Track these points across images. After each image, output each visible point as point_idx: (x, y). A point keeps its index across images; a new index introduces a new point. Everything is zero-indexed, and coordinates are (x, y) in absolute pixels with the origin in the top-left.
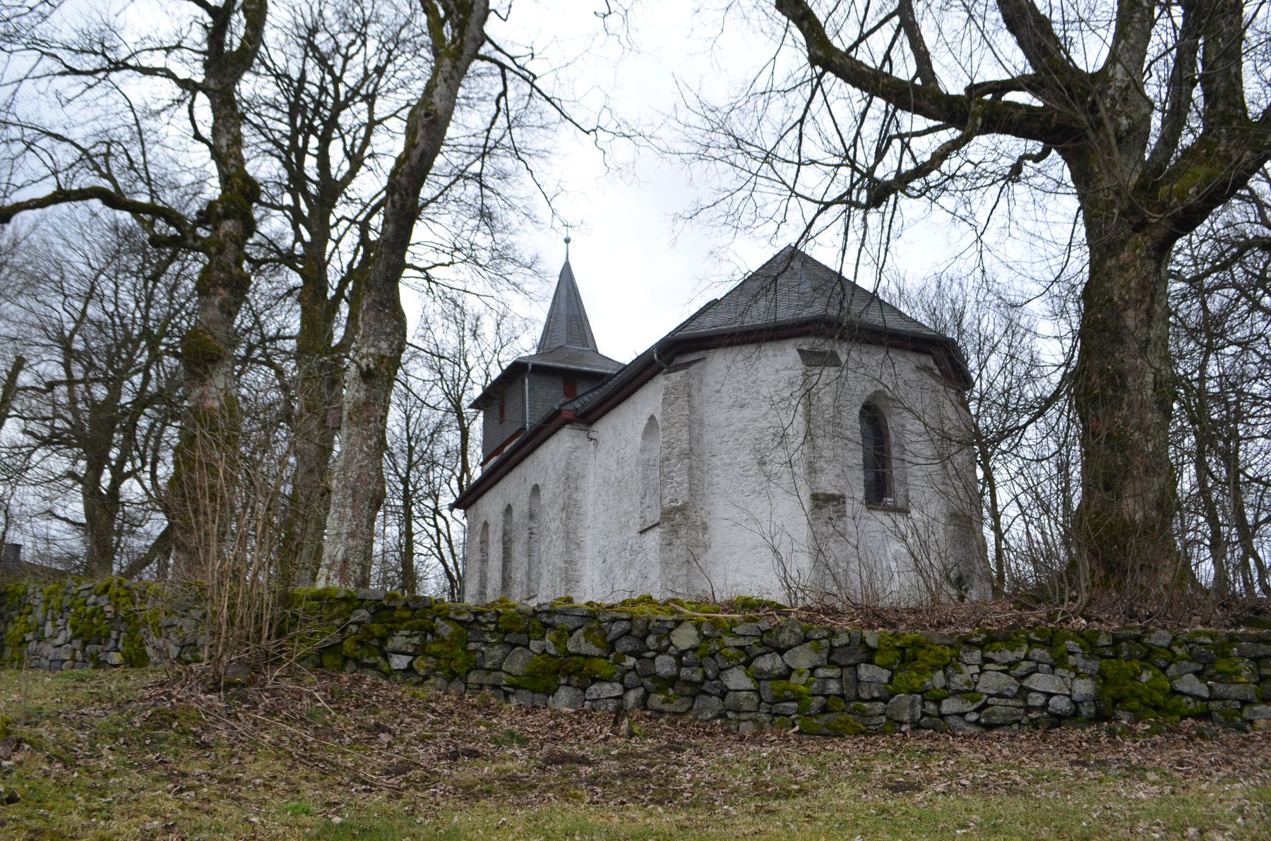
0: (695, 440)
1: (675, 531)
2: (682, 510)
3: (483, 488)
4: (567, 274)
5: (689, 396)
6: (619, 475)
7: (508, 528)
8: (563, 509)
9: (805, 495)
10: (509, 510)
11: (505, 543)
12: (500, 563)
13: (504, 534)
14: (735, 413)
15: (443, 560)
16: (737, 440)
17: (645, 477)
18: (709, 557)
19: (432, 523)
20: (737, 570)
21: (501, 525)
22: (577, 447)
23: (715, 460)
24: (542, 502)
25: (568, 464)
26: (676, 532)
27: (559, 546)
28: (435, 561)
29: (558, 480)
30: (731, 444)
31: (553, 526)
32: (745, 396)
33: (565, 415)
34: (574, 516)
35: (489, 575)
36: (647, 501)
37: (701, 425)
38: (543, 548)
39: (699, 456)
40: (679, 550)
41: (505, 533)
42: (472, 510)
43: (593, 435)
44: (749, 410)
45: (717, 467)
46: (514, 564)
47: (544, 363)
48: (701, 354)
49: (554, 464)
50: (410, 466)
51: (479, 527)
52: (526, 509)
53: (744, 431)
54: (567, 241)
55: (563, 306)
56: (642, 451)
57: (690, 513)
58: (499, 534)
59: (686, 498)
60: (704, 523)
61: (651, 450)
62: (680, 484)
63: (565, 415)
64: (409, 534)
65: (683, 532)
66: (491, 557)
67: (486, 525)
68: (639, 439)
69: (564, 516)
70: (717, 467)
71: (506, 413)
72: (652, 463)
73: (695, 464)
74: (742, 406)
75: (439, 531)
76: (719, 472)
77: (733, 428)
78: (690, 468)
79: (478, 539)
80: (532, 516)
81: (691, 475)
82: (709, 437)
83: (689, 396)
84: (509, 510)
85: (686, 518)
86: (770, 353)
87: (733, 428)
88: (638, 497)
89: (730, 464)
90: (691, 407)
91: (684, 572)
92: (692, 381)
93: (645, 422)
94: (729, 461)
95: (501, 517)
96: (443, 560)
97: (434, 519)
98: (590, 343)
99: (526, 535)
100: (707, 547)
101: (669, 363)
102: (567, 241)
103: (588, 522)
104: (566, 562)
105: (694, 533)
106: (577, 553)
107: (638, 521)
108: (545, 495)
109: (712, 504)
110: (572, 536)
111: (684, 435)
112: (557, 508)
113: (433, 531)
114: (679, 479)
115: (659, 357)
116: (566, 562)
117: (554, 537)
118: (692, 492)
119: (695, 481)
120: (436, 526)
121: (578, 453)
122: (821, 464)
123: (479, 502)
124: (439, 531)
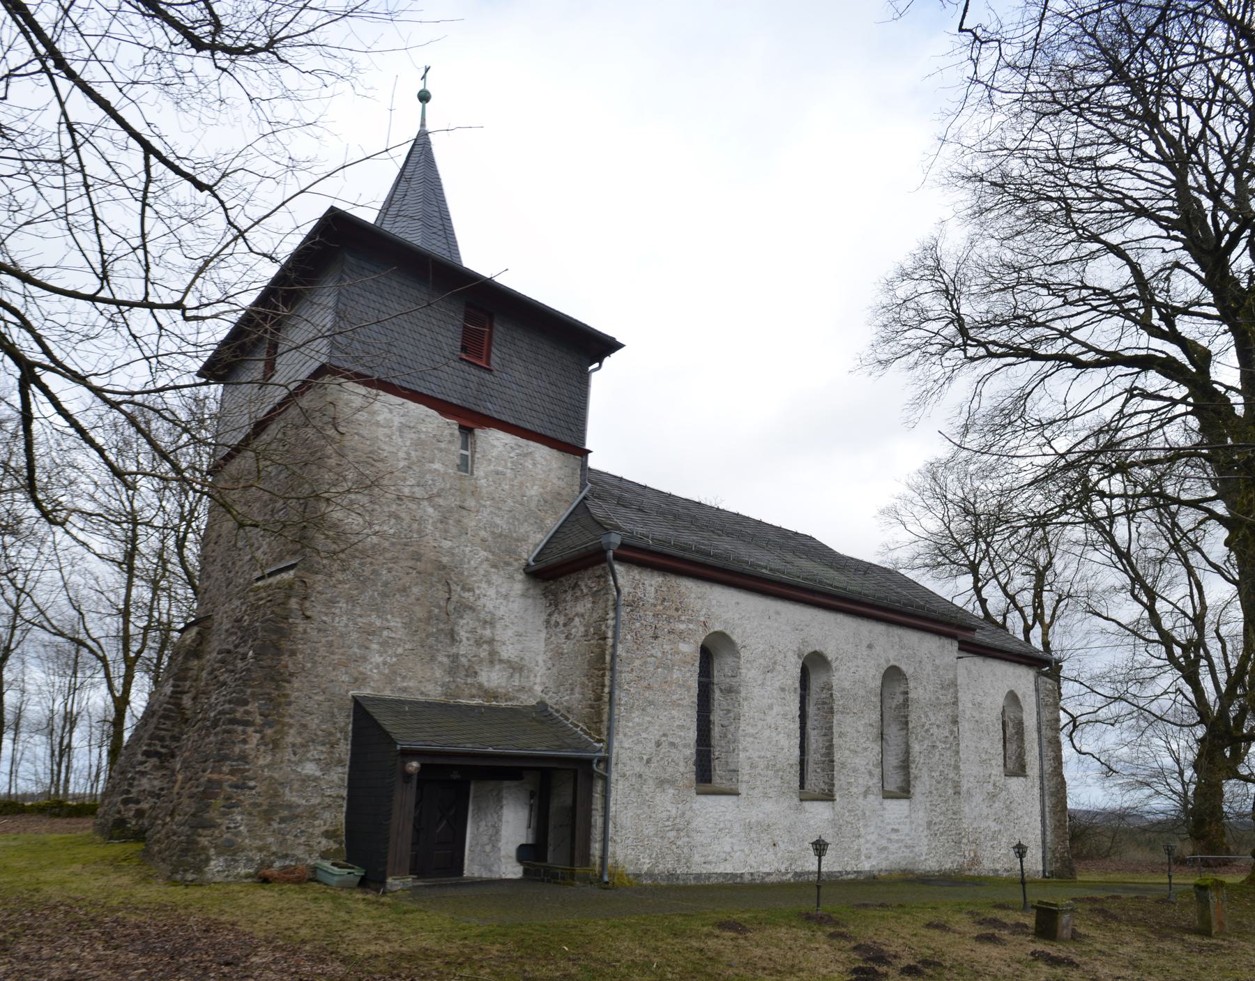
4: (421, 149)
117: (940, 745)
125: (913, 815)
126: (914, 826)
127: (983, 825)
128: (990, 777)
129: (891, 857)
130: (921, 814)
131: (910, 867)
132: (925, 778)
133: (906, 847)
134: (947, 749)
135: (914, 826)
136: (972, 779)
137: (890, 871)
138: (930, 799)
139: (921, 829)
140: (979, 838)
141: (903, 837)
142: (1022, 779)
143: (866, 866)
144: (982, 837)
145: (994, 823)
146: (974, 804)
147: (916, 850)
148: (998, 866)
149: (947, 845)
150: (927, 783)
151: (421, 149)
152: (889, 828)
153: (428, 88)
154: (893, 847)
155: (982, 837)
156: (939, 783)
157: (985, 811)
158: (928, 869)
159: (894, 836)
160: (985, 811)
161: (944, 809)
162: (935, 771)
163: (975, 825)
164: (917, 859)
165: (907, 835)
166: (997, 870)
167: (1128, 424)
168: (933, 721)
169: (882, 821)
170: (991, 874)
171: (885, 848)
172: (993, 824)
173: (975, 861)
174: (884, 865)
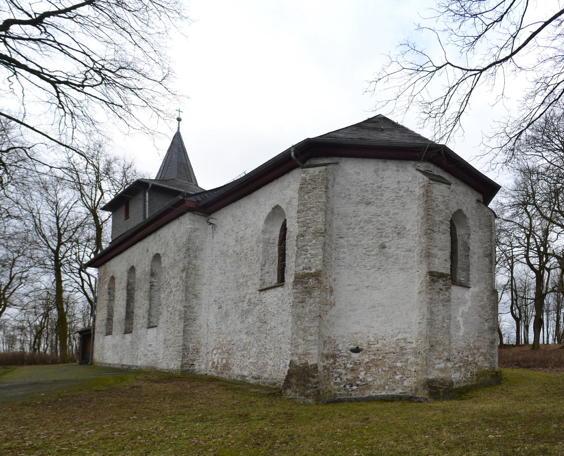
0: (328, 223)
1: (308, 292)
2: (317, 275)
3: (110, 255)
4: (178, 138)
5: (327, 188)
6: (238, 249)
7: (131, 281)
8: (183, 271)
9: (424, 270)
10: (132, 270)
11: (128, 290)
12: (125, 303)
13: (128, 285)
14: (362, 208)
15: (85, 294)
16: (362, 228)
17: (265, 251)
18: (333, 312)
19: (78, 276)
20: (358, 323)
21: (125, 279)
22: (197, 229)
23: (342, 241)
24: (163, 265)
25: (189, 240)
26: (309, 293)
27: (179, 295)
28: (80, 294)
29: (179, 250)
30: (356, 231)
31: (173, 282)
32: (370, 196)
33: (187, 204)
34: (193, 276)
35: (115, 309)
36: (267, 268)
37: (333, 213)
38: (163, 296)
39: (330, 236)
40: (312, 305)
41: (129, 284)
42: (102, 268)
43: (212, 221)
44: (374, 207)
45: (344, 246)
46: (137, 304)
47: (160, 184)
48: (335, 159)
49: (176, 240)
50: (60, 244)
51: (107, 279)
52: (148, 269)
53: (369, 221)
54: (179, 120)
55: (175, 157)
56: (264, 232)
57: (322, 279)
58: (124, 284)
59: (319, 267)
60: (331, 287)
61: (271, 232)
62: (316, 255)
63: (187, 204)
64: (59, 281)
65: (316, 293)
66: (117, 298)
67: (113, 278)
68: (261, 224)
69: (184, 275)
70: (344, 246)
71: (131, 214)
72: (271, 241)
73: (327, 241)
74: (368, 204)
75: (83, 280)
76: (345, 250)
77: (359, 219)
78: (324, 244)
79: (106, 286)
80: (152, 274)
81: (324, 250)
82: (337, 223)
83: (327, 188)
84: (132, 270)
85: (320, 282)
86: (395, 168)
87: (359, 219)
88: (258, 266)
89: (356, 245)
90: (327, 197)
91: (317, 324)
92: (329, 177)
93: (269, 210)
94: (355, 243)
95: (126, 274)
96: (85, 294)
97: (80, 274)
98: (193, 181)
99: (147, 286)
100: (333, 305)
101: (304, 162)
102: (179, 120)
103: (205, 281)
104: (185, 307)
105: (324, 294)
106: (195, 301)
107: (257, 280)
108: (166, 262)
109: (338, 273)
110: (190, 289)
111: (320, 217)
112: (176, 270)
113: (79, 280)
114: (313, 252)
115: (296, 155)
116: (185, 307)
117: (174, 290)
118: (325, 262)
119: (327, 255)
120: (81, 277)
121: (198, 233)
122: (435, 251)
123: (108, 264)
124: (83, 280)
125: (158, 336)
126: (158, 342)
127: (236, 338)
128: (245, 297)
129: (148, 360)
130: (161, 335)
131: (154, 366)
132: (165, 313)
133: (154, 354)
134: (178, 290)
135: (158, 342)
136: (229, 302)
137: (147, 367)
138: (166, 325)
139: (161, 344)
140: (232, 349)
141: (153, 349)
142: (434, 270)
143: (139, 363)
144: (235, 348)
145: (245, 336)
146: (229, 322)
147: (158, 356)
148: (246, 373)
149: (172, 353)
150: (166, 316)
151: (178, 138)
152: (148, 344)
153: (180, 117)
154: (149, 354)
155: (235, 348)
156: (171, 314)
157: (239, 326)
158: (162, 367)
159: (150, 349)
160: (239, 326)
161: (173, 330)
162: (170, 307)
163: (229, 339)
164: (158, 361)
165: (155, 348)
166: (243, 376)
167: (76, 47)
168: (172, 276)
169: (146, 341)
170: (239, 379)
171: (146, 355)
172: (244, 336)
173: (226, 367)
174: (145, 364)
